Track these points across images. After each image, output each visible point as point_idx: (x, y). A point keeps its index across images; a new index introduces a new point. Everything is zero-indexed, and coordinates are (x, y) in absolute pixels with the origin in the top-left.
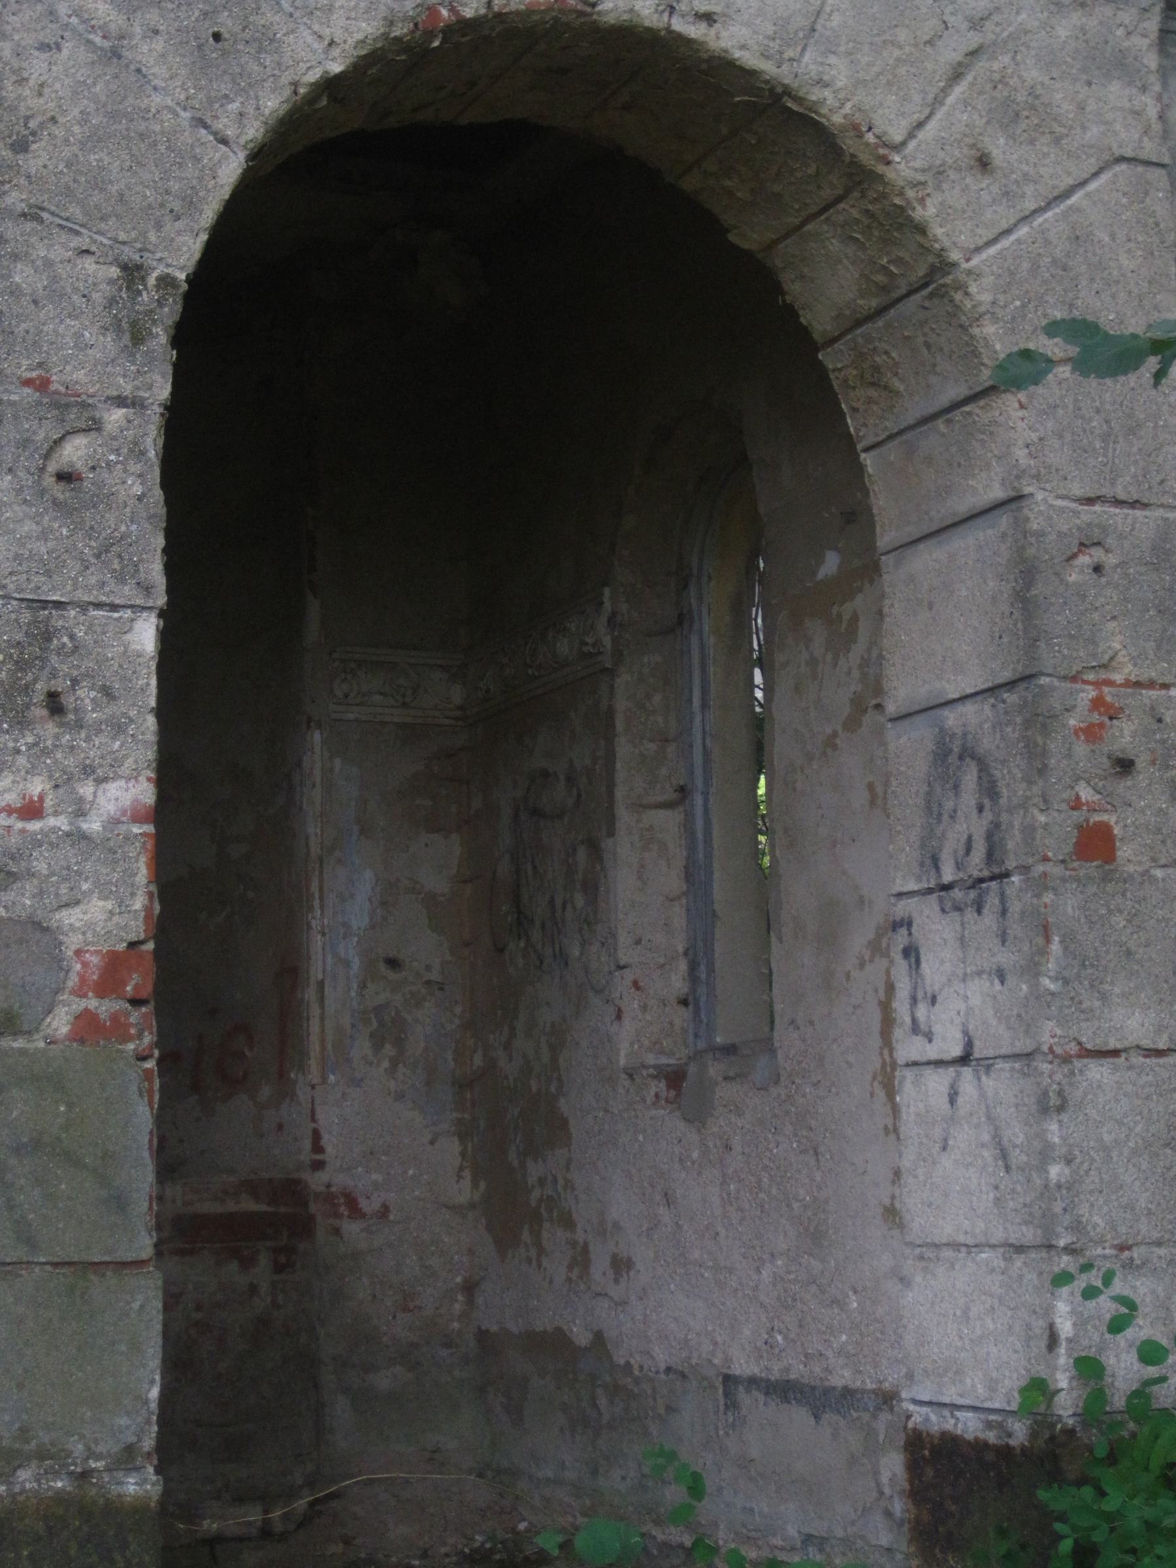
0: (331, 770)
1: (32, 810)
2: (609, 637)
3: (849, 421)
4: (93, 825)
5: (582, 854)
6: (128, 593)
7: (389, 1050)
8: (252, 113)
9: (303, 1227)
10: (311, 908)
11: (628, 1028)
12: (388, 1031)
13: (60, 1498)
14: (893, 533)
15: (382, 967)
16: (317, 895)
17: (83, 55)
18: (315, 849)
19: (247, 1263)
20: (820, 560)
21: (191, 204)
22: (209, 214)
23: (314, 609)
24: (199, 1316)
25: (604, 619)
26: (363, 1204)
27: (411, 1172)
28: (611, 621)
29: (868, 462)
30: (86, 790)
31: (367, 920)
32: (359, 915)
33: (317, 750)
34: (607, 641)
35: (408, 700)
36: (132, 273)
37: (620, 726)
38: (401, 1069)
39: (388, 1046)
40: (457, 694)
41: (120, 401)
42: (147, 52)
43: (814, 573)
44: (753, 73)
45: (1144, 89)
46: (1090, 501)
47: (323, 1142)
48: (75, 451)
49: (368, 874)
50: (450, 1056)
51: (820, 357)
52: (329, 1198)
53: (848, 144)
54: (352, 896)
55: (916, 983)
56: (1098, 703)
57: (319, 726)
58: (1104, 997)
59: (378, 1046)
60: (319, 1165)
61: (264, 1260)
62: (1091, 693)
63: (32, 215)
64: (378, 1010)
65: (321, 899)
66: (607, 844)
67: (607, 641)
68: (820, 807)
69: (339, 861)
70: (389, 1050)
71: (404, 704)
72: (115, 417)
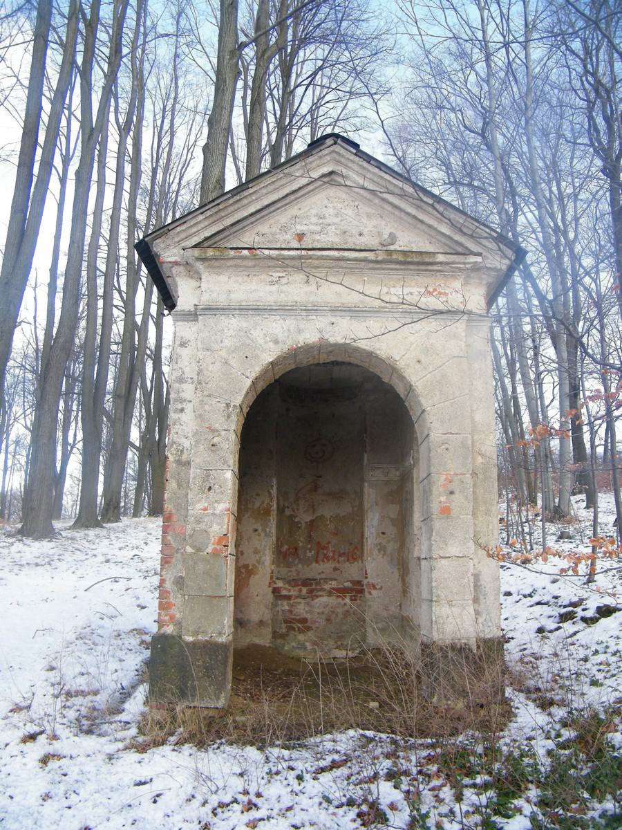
1: (205, 509)
4: (217, 512)
6: (225, 467)
7: (382, 552)
8: (255, 371)
9: (361, 591)
12: (382, 549)
13: (206, 641)
17: (220, 364)
21: (240, 390)
22: (244, 392)
23: (366, 456)
30: (216, 505)
32: (375, 523)
36: (228, 405)
40: (398, 473)
41: (225, 430)
42: (232, 362)
44: (364, 350)
45: (461, 340)
46: (445, 434)
48: (216, 440)
49: (378, 514)
52: (368, 584)
53: (387, 361)
56: (446, 479)
58: (446, 545)
59: (379, 552)
60: (366, 578)
61: (348, 597)
62: (445, 477)
63: (209, 396)
64: (380, 544)
67: (412, 462)
70: (382, 552)
72: (223, 433)
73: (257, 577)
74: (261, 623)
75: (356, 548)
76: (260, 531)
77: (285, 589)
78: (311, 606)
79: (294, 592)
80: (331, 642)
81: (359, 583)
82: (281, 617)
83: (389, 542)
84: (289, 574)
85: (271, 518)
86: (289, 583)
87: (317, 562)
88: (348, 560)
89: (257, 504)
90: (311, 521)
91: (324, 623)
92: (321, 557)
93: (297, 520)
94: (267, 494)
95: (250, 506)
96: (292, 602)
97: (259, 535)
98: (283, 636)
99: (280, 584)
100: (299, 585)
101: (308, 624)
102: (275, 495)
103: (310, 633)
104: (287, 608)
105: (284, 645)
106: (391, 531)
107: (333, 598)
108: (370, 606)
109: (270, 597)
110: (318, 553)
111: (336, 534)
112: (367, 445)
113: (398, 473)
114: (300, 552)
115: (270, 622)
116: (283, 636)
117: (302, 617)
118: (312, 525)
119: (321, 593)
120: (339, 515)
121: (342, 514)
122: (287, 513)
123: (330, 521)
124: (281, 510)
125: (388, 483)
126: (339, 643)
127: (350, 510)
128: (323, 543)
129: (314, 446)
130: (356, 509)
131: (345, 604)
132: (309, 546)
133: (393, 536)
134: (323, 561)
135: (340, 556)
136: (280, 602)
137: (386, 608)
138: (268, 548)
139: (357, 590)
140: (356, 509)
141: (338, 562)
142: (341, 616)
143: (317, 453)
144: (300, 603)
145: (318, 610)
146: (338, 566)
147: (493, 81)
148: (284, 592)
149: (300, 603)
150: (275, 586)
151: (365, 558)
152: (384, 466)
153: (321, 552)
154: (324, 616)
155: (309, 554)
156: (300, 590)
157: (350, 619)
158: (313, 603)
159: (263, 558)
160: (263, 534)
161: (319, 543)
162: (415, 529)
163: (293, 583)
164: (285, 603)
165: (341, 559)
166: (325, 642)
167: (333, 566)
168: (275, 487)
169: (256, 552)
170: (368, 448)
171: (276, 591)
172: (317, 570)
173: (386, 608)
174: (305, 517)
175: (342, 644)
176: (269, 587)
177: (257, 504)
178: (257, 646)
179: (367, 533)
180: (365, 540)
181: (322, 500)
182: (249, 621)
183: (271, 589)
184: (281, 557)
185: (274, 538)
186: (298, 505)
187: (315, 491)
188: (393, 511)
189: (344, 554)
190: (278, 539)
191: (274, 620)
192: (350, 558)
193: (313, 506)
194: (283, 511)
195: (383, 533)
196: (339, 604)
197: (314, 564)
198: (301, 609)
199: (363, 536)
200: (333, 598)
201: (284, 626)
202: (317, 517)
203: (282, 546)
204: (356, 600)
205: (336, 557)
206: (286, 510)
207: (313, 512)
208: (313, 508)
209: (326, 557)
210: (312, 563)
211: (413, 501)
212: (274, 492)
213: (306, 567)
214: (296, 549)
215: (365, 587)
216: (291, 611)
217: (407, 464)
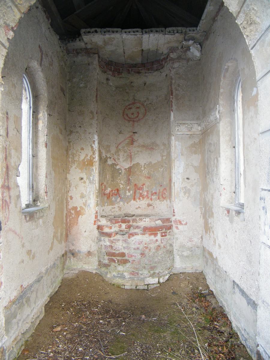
0: (176, 144)
2: (218, 115)
3: (246, 41)
5: (216, 161)
7: (187, 195)
9: (170, 228)
10: (172, 169)
11: (223, 198)
12: (187, 191)
14: (260, 74)
15: (186, 180)
16: (173, 167)
18: (173, 159)
19: (156, 235)
20: (253, 91)
23: (172, 114)
24: (146, 245)
25: (217, 112)
26: (182, 222)
27: (191, 217)
28: (219, 112)
29: (253, 53)
31: (183, 171)
32: (181, 170)
33: (173, 140)
34: (218, 116)
35: (190, 130)
37: (221, 134)
38: (189, 198)
39: (187, 194)
40: (199, 128)
43: (252, 94)
47: (175, 211)
49: (183, 163)
50: (199, 196)
51: (236, 21)
52: (176, 221)
54: (180, 167)
55: (266, 219)
57: (173, 136)
59: (185, 194)
60: (174, 215)
61: (159, 235)
64: (185, 187)
65: (174, 167)
66: (219, 159)
67: (218, 116)
68: (253, 155)
69: (177, 160)
71: (189, 131)
73: (84, 216)
74: (89, 253)
75: (165, 189)
76: (85, 179)
77: (107, 226)
78: (128, 243)
79: (115, 228)
80: (145, 272)
81: (168, 220)
82: (104, 251)
83: (192, 186)
84: (113, 210)
85: (94, 168)
86: (110, 220)
87: (134, 199)
88: (159, 198)
89: (82, 157)
90: (128, 168)
91: (140, 257)
92: (138, 195)
93: (118, 167)
94: (90, 148)
95: (76, 158)
96: (112, 239)
97: (85, 182)
98: (107, 266)
99: (103, 222)
100: (118, 222)
101: (126, 258)
102: (97, 149)
103: (128, 265)
104: (108, 244)
105: (107, 273)
106: (195, 176)
107: (147, 235)
108: (177, 239)
109: (96, 232)
110: (135, 193)
111: (149, 178)
112: (173, 104)
113: (199, 128)
114: (121, 192)
115: (96, 252)
116: (107, 266)
117: (121, 251)
118: (130, 171)
119: (136, 231)
120: (151, 163)
121: (154, 162)
122: (110, 162)
123: (145, 168)
124: (103, 161)
125: (191, 136)
126: (152, 272)
127: (160, 159)
128: (140, 185)
129: (131, 108)
130: (164, 158)
131: (157, 240)
132: (128, 187)
133: (196, 181)
134: (139, 199)
135: (152, 195)
136: (102, 238)
137: (191, 240)
138: (92, 193)
139: (165, 227)
140: (164, 158)
141: (151, 199)
142: (153, 251)
143: (133, 114)
144: (119, 240)
145: (133, 246)
146: (151, 202)
147: (115, 292)
148: (106, 230)
149: (119, 240)
150: (99, 223)
151: (173, 199)
152: (188, 122)
153: (137, 192)
154: (139, 252)
155: (128, 194)
156: (120, 226)
157: (160, 252)
158: (130, 240)
159: (89, 202)
160: (87, 182)
161: (135, 185)
162: (222, 180)
163: (114, 220)
164: (107, 239)
165: (153, 197)
166: (141, 272)
167: (147, 202)
168: (96, 142)
169: (82, 196)
170: (174, 107)
171: (99, 228)
172: (135, 206)
173: (191, 240)
174: (124, 165)
175: (154, 273)
176: (95, 224)
177: (82, 157)
178: (85, 274)
179: (174, 179)
180: (172, 185)
181: (138, 151)
182: (79, 252)
183: (96, 226)
184: (106, 198)
185: (97, 185)
186: (119, 155)
187: (132, 144)
188: (196, 159)
189: (156, 193)
190: (101, 184)
191: (99, 252)
192: (161, 197)
193: (131, 157)
194: (106, 161)
195: (188, 179)
196: (152, 240)
197: (132, 201)
198: (120, 246)
199: (170, 180)
200: (147, 235)
201: (106, 257)
202: (134, 165)
203: (106, 188)
204: (165, 236)
205: (150, 195)
206: (109, 160)
207: (131, 161)
208: (130, 157)
209: (141, 195)
210: (130, 201)
211: (219, 153)
212: (96, 146)
213: (126, 204)
214: (118, 190)
215: (173, 223)
216: (111, 247)
217: (212, 118)
